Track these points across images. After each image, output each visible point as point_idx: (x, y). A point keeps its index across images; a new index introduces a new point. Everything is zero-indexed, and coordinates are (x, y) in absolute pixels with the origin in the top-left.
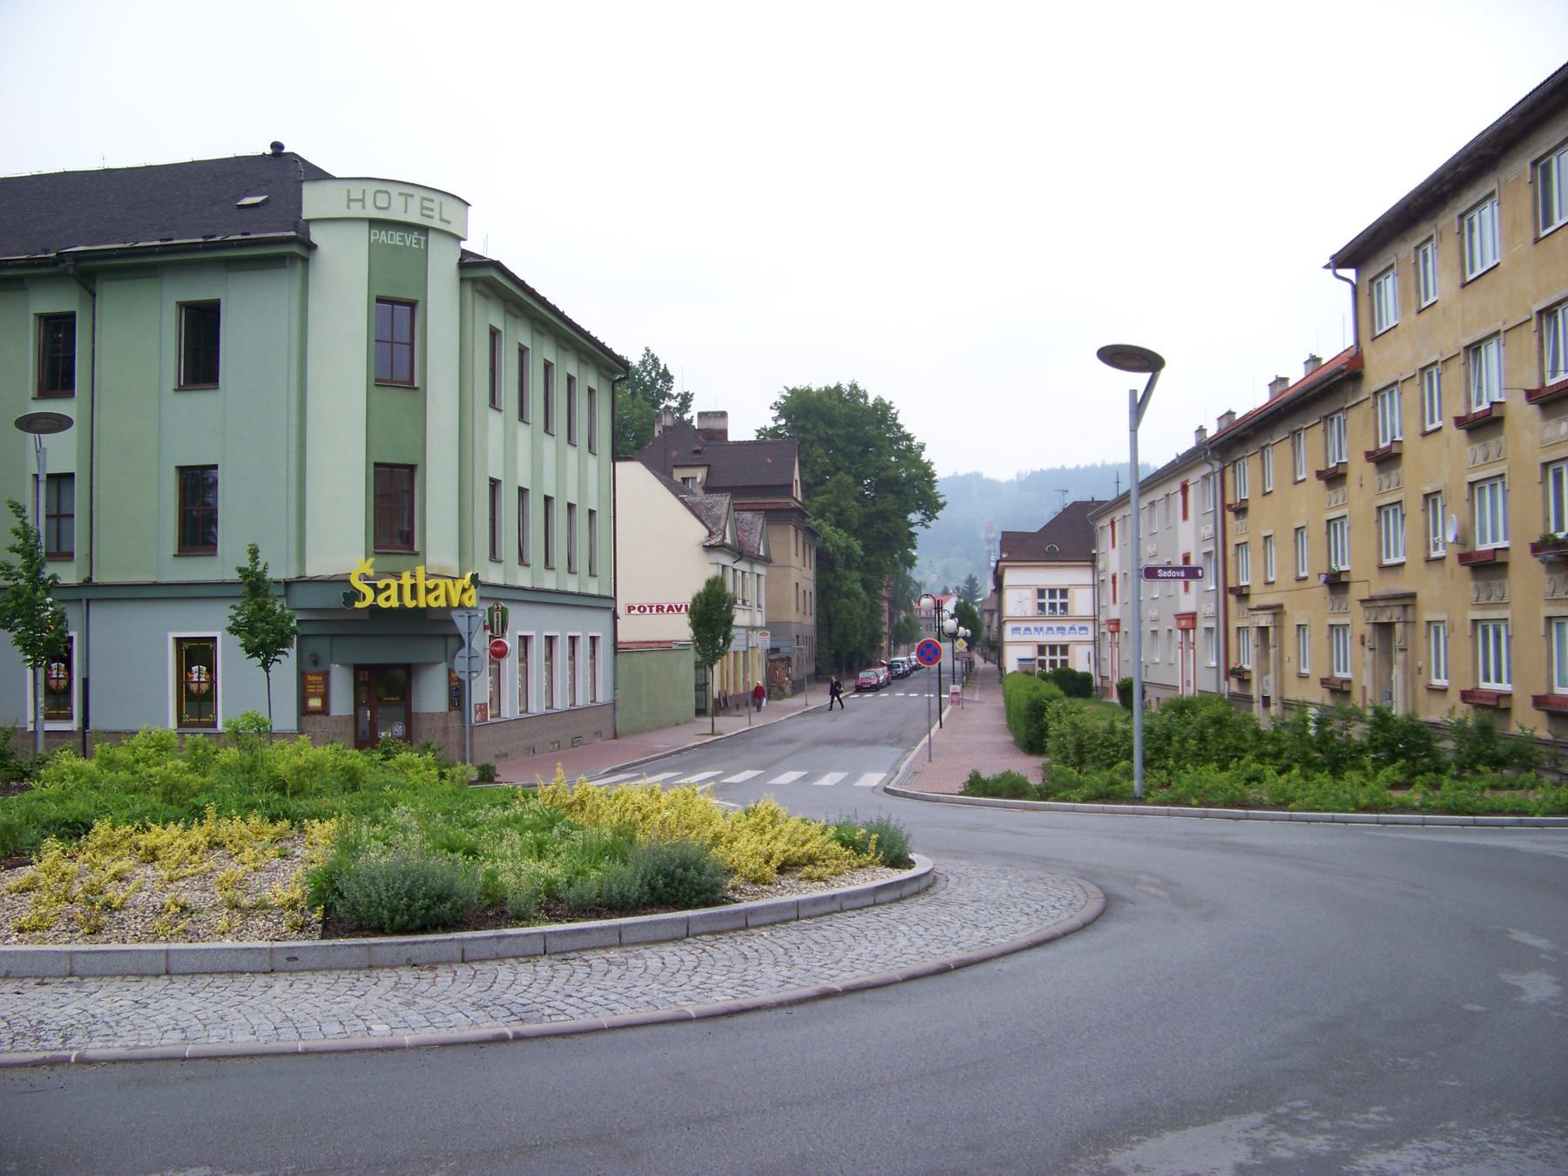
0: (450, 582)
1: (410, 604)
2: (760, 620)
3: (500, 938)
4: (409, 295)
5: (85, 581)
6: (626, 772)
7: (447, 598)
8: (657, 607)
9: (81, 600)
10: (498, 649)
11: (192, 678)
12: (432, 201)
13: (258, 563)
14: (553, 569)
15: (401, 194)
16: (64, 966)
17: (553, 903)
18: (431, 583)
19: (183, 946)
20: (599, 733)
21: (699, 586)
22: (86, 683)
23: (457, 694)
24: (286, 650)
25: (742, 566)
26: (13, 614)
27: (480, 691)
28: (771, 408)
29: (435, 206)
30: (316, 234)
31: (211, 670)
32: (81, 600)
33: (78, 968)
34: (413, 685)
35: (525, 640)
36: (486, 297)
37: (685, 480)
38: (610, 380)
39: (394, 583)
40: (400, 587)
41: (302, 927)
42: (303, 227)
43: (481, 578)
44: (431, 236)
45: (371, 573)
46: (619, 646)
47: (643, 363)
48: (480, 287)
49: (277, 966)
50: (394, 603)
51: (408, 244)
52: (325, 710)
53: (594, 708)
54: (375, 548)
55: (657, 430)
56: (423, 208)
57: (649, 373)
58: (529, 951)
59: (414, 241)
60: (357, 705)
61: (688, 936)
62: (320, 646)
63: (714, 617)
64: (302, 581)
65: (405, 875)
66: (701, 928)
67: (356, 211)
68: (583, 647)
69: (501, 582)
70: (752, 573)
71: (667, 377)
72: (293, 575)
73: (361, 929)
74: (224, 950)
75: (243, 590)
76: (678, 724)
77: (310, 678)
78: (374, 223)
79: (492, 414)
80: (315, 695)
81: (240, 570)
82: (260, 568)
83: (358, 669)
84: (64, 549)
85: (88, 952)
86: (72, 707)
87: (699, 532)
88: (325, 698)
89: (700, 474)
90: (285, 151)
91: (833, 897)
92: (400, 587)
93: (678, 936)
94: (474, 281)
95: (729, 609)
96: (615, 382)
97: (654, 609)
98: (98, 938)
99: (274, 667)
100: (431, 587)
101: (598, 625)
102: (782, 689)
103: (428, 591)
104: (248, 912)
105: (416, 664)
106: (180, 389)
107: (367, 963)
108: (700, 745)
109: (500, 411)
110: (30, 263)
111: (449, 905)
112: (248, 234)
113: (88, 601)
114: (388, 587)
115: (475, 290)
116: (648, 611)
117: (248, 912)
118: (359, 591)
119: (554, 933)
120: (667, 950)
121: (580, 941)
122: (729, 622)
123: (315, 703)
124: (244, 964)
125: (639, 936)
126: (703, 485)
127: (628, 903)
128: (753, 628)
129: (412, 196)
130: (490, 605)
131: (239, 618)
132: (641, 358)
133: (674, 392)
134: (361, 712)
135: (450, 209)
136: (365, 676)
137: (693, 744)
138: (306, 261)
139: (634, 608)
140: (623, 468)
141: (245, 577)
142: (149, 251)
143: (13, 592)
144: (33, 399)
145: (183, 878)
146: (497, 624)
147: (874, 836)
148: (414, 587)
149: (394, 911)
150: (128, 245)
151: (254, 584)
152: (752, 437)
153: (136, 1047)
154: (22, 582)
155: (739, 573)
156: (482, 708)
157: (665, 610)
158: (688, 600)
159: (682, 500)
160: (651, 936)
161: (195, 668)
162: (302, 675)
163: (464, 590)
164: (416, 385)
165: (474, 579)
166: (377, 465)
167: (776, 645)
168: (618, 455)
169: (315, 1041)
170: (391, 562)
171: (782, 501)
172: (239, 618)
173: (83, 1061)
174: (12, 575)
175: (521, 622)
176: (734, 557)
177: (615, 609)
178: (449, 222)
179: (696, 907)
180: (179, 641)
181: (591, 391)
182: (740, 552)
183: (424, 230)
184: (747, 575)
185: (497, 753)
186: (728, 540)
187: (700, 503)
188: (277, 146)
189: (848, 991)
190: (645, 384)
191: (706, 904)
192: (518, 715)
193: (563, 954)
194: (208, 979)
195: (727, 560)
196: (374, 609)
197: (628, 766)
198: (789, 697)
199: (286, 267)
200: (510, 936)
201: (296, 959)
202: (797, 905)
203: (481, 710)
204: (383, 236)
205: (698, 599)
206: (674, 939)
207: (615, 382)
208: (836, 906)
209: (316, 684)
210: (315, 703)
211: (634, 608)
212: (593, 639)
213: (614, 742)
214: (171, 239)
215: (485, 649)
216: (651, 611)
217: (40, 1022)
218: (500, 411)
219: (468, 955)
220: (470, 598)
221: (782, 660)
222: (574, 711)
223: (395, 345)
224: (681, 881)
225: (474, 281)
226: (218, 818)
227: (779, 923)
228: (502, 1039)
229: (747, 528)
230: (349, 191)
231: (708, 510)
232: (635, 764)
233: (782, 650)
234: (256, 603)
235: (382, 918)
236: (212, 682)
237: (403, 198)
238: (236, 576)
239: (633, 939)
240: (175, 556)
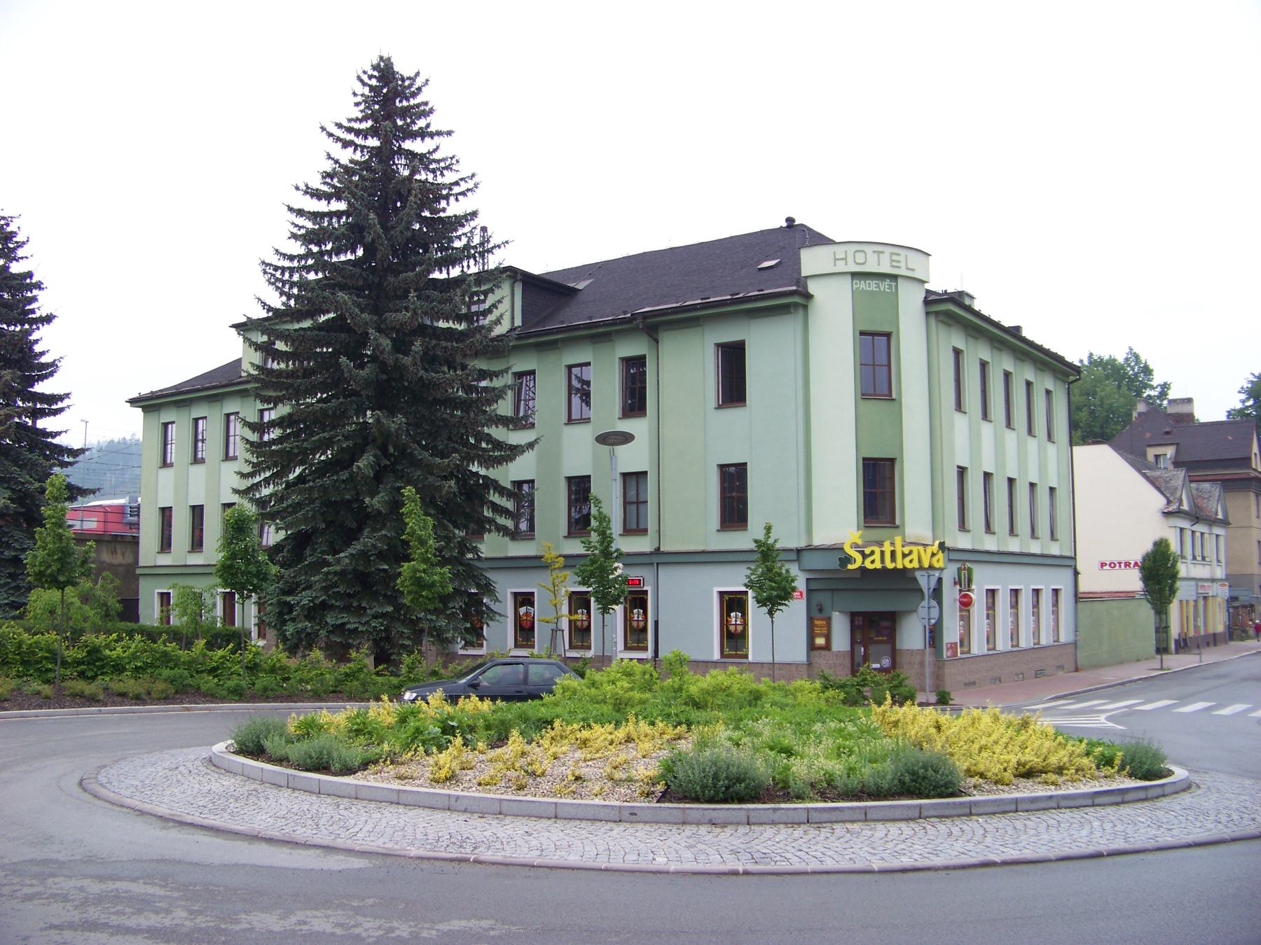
0: (921, 548)
1: (890, 565)
2: (1219, 573)
3: (774, 809)
4: (886, 329)
5: (656, 550)
6: (1068, 699)
7: (920, 561)
8: (1125, 563)
9: (653, 564)
10: (965, 600)
11: (731, 621)
12: (899, 255)
13: (769, 537)
14: (1017, 536)
15: (874, 252)
16: (496, 807)
17: (827, 789)
18: (906, 550)
19: (569, 801)
20: (1061, 667)
21: (1148, 547)
22: (656, 623)
23: (934, 634)
24: (786, 602)
25: (1200, 528)
26: (590, 575)
27: (951, 633)
28: (1240, 392)
29: (901, 258)
30: (812, 287)
31: (744, 615)
32: (653, 564)
33: (504, 810)
34: (897, 628)
35: (992, 593)
36: (949, 325)
37: (1157, 457)
38: (1065, 382)
39: (877, 550)
40: (882, 553)
41: (647, 794)
42: (801, 282)
43: (947, 545)
44: (900, 281)
45: (860, 542)
46: (1080, 595)
47: (1127, 359)
48: (941, 318)
49: (624, 818)
50: (878, 565)
51: (882, 289)
52: (827, 647)
53: (1057, 646)
54: (865, 523)
55: (1135, 414)
56: (892, 261)
57: (1133, 369)
58: (796, 820)
59: (887, 287)
60: (853, 643)
61: (920, 818)
62: (824, 598)
63: (1160, 573)
64: (811, 549)
65: (715, 764)
66: (932, 813)
67: (841, 267)
68: (1046, 599)
69: (969, 547)
70: (1210, 534)
71: (1147, 371)
72: (802, 544)
73: (685, 798)
74: (594, 805)
75: (757, 556)
76: (1138, 661)
77: (817, 622)
78: (854, 275)
79: (958, 416)
80: (820, 635)
81: (756, 541)
82: (770, 541)
83: (853, 616)
84: (642, 527)
85: (510, 800)
86: (647, 641)
87: (1159, 501)
88: (828, 638)
89: (1170, 452)
90: (796, 223)
91: (1051, 797)
92: (882, 553)
93: (912, 817)
94: (937, 313)
95: (1174, 565)
96: (1069, 383)
97: (1123, 565)
98: (521, 792)
99: (777, 614)
100: (907, 552)
101: (1061, 579)
102: (1245, 632)
103: (904, 556)
104: (617, 783)
105: (899, 612)
106: (719, 407)
107: (681, 821)
108: (1145, 678)
109: (965, 413)
110: (614, 322)
111: (743, 785)
112: (762, 290)
113: (658, 564)
114: (872, 553)
115: (938, 321)
116: (1117, 567)
117: (617, 783)
118: (851, 557)
119: (816, 809)
120: (903, 825)
121: (834, 816)
122: (1174, 576)
123: (820, 641)
124: (602, 816)
125: (880, 815)
126: (1173, 460)
127: (881, 792)
128: (1213, 580)
129: (883, 252)
130: (958, 565)
131: (753, 577)
132: (1125, 356)
133: (1154, 383)
134: (857, 647)
135: (914, 259)
136: (859, 620)
137: (1138, 677)
138: (805, 307)
139: (1106, 564)
140: (1081, 452)
141: (759, 547)
142: (693, 308)
143: (591, 559)
144: (619, 418)
145: (594, 759)
146: (964, 581)
147: (1119, 754)
148: (893, 553)
149: (704, 787)
150: (678, 305)
151: (766, 553)
152: (1222, 417)
153: (510, 857)
154: (597, 552)
155: (1198, 534)
156: (953, 646)
157: (1132, 566)
158: (1139, 559)
159: (1145, 476)
160: (891, 816)
161: (733, 614)
162: (810, 620)
163: (933, 555)
164: (894, 397)
165: (942, 546)
166: (864, 459)
167: (1235, 594)
168: (1072, 443)
169: (616, 863)
170: (875, 534)
171: (1241, 472)
172: (753, 577)
173: (477, 861)
174: (591, 547)
175: (984, 579)
176: (1192, 520)
177: (1075, 566)
178: (913, 270)
179: (934, 797)
180: (721, 594)
181: (1048, 392)
182: (1196, 516)
183: (894, 277)
184: (1206, 536)
185: (966, 681)
186: (1185, 507)
187: (1160, 477)
188: (790, 220)
189: (1005, 863)
190: (1129, 378)
191: (941, 796)
192: (986, 652)
193: (819, 824)
194: (578, 822)
195: (1185, 524)
196: (863, 570)
197: (1072, 694)
198: (1252, 638)
199: (791, 313)
200: (783, 809)
201: (636, 814)
202: (1016, 801)
203: (951, 648)
204: (862, 285)
205: (1147, 558)
206: (908, 820)
207: (1069, 383)
208: (1053, 804)
209: (821, 627)
210: (820, 641)
211: (1106, 564)
212: (1056, 591)
213: (1077, 673)
214: (709, 298)
215: (955, 600)
216: (1120, 566)
217: (468, 838)
218: (965, 413)
219: (752, 820)
220: (938, 561)
221: (1244, 607)
222: (1037, 649)
223: (876, 367)
224: (924, 778)
225: (937, 313)
226: (637, 722)
227: (999, 813)
228: (735, 873)
229: (1206, 496)
230: (835, 253)
231: (1166, 482)
232: (1078, 693)
233: (1240, 598)
234: (766, 566)
235: (697, 792)
236: (745, 624)
237: (876, 255)
238: (753, 546)
239: (875, 817)
240: (718, 531)
